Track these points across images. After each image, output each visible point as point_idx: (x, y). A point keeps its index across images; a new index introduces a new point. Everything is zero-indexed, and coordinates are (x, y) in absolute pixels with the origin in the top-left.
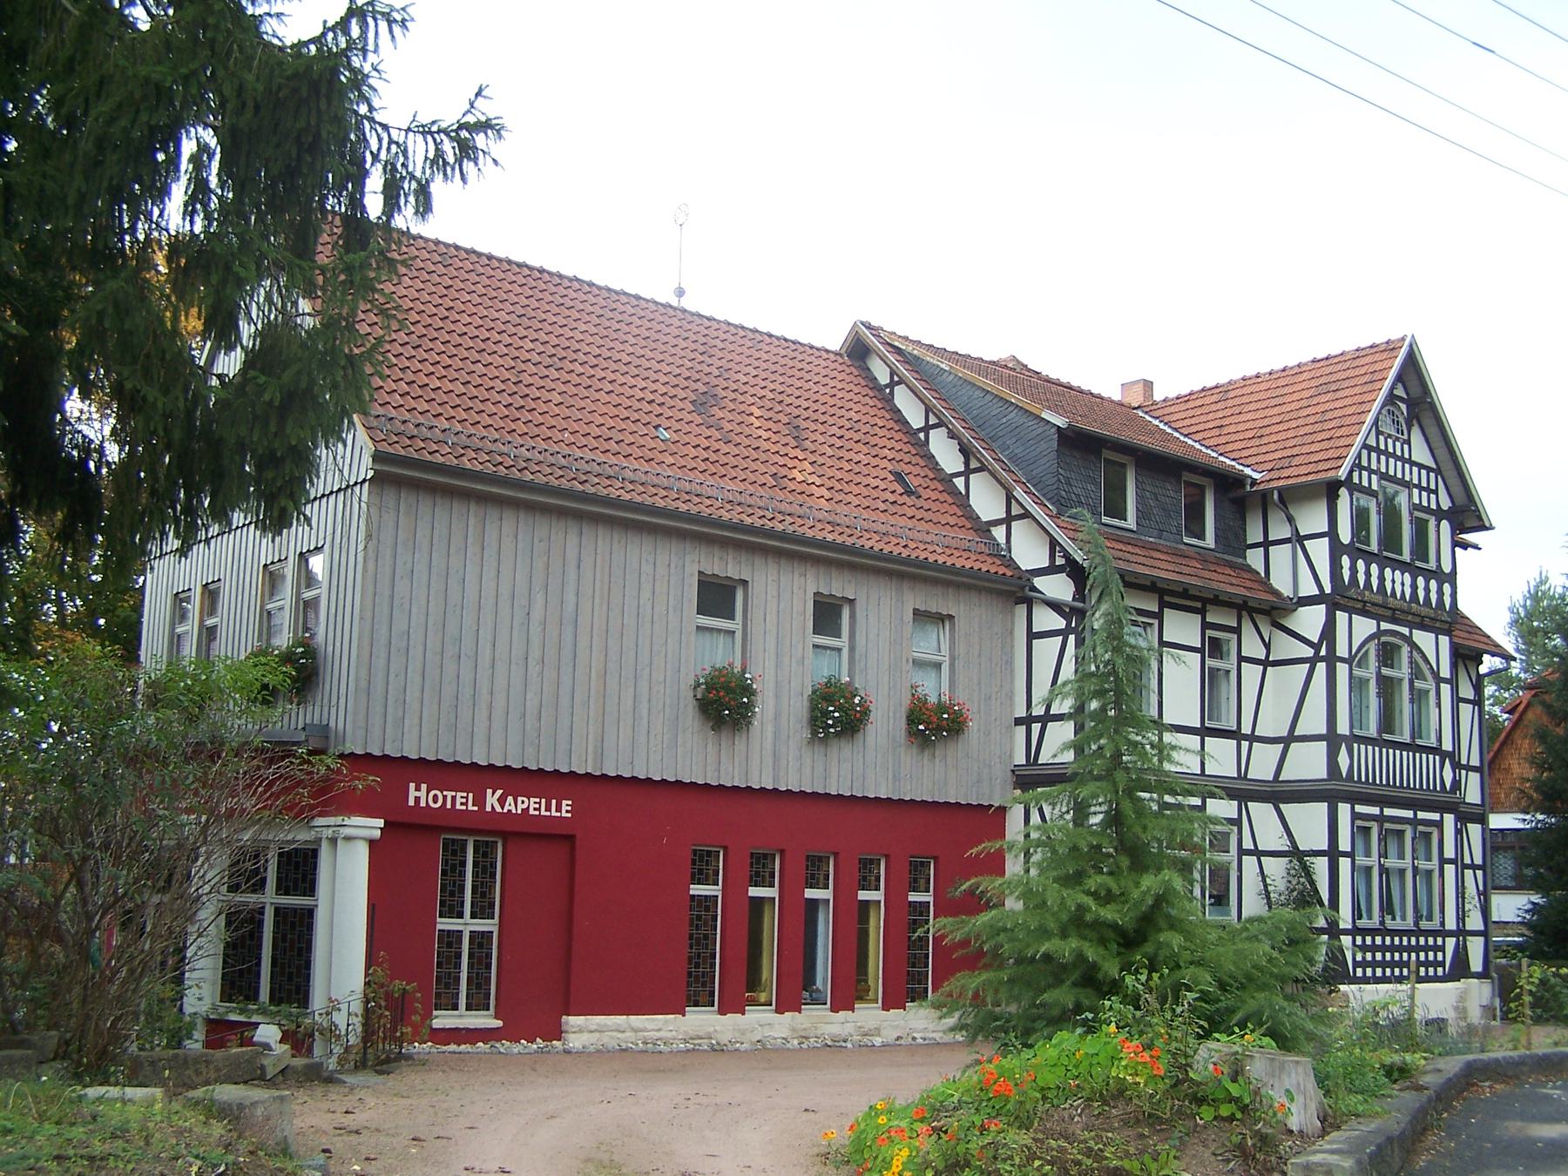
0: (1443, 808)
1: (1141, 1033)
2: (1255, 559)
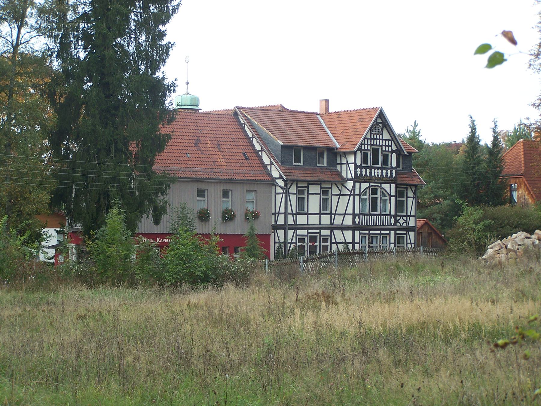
0: (390, 230)
1: (481, 363)
2: (338, 167)
